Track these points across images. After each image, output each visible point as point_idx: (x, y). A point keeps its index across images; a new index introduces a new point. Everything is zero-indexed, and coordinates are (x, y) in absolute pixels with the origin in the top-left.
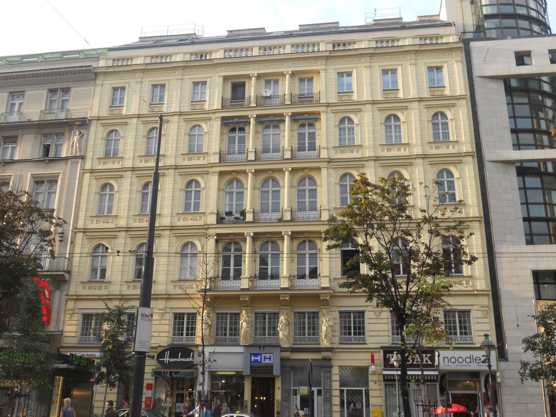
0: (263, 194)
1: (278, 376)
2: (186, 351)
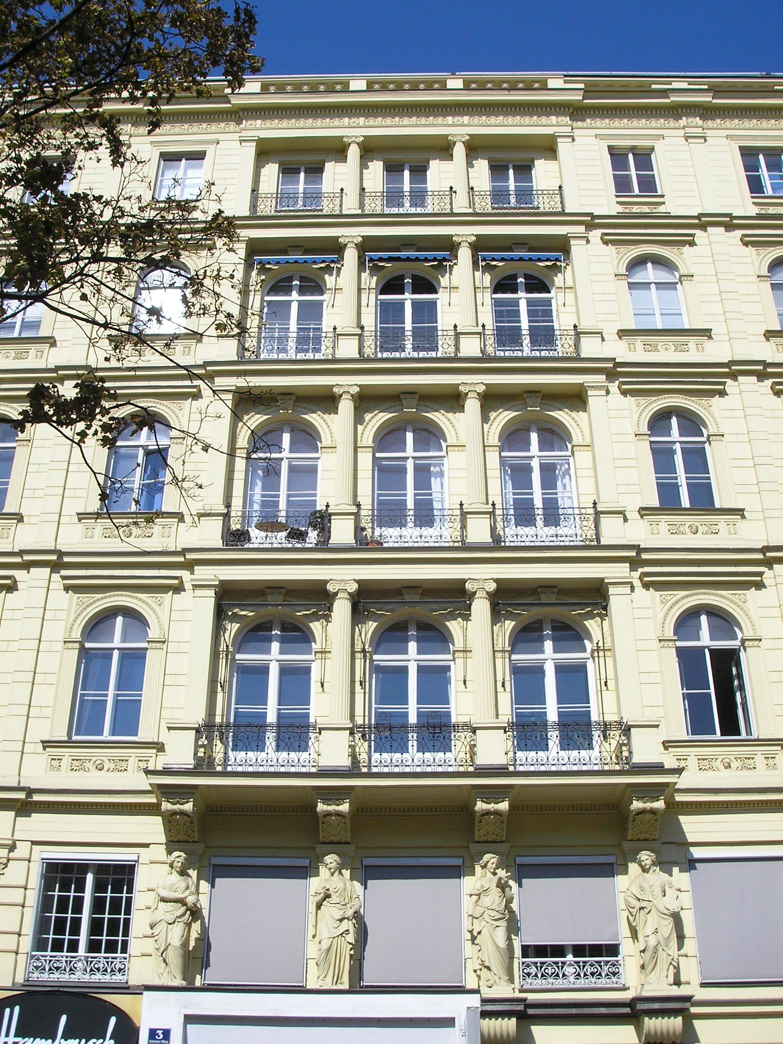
2: (499, 287)
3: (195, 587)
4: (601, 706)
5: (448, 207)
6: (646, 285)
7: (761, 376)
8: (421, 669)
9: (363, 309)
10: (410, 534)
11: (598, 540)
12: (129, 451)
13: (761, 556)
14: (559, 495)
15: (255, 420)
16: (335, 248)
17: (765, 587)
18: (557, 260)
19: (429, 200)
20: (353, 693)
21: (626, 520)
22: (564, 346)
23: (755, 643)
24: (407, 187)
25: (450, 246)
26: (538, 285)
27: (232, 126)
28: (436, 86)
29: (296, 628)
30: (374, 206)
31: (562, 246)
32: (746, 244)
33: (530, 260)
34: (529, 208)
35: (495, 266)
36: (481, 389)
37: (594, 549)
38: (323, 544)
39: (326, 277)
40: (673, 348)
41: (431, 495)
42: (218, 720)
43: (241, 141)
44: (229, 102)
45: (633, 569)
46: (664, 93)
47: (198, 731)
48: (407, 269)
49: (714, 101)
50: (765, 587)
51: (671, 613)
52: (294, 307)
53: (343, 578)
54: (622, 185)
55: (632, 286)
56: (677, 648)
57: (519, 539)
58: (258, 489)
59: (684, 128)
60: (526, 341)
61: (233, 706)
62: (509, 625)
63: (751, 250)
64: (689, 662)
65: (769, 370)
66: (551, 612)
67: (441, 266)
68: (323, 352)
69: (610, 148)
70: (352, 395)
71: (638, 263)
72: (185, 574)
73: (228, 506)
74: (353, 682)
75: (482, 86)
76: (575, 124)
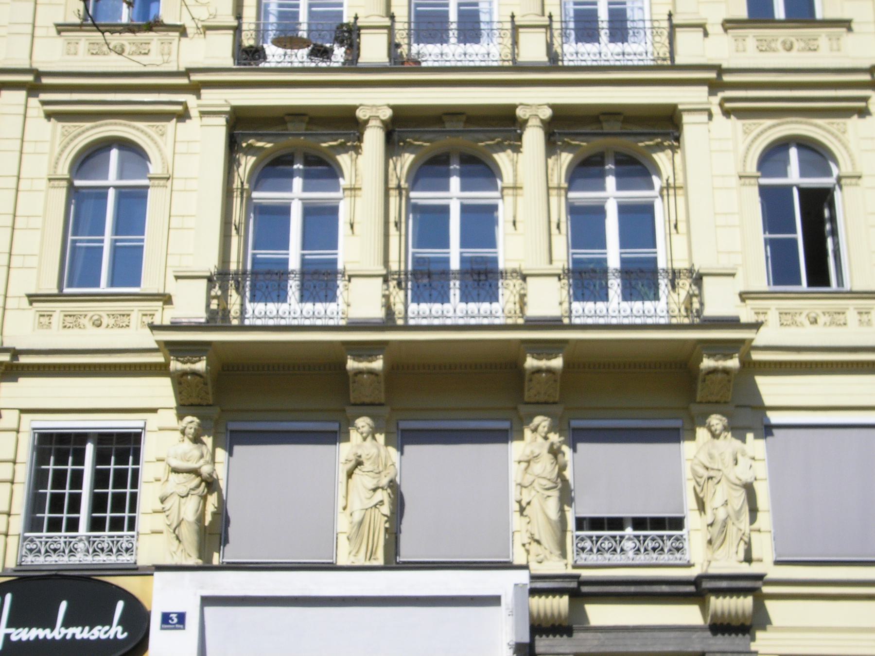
0: (209, 610)
1: (392, 189)
2: (91, 594)
3: (203, 114)
8: (466, 210)
10: (452, 52)
11: (672, 58)
23: (854, 181)
29: (320, 161)
37: (669, 71)
38: (352, 64)
42: (233, 267)
47: (210, 279)
53: (375, 103)
64: (774, 202)
72: (190, 99)
74: (549, 222)
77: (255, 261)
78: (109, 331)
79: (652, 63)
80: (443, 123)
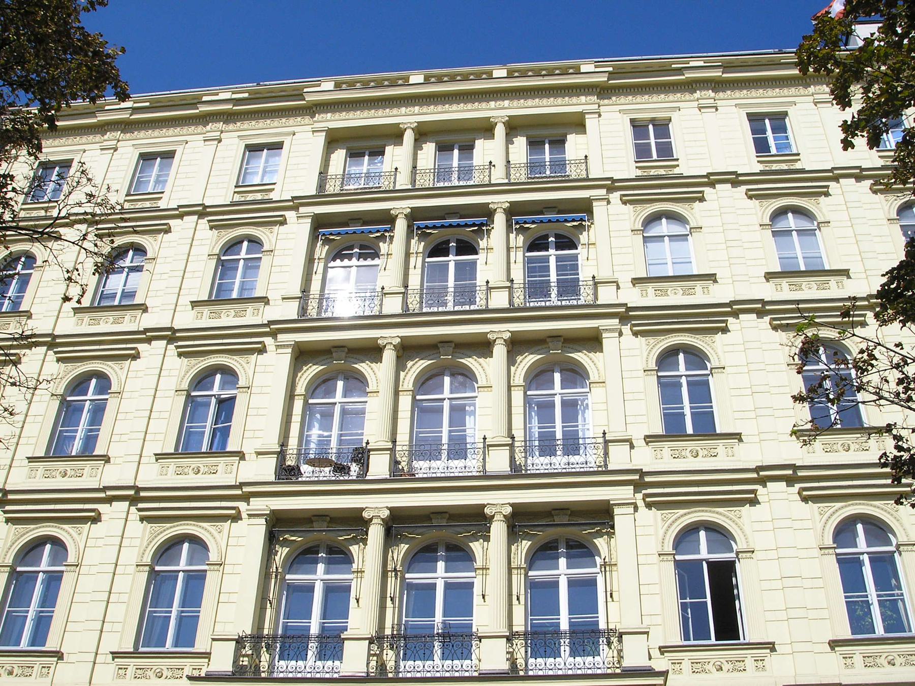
3: (250, 516)
4: (608, 616)
5: (584, 173)
6: (788, 233)
7: (760, 313)
8: (448, 586)
9: (512, 265)
10: (440, 466)
11: (606, 465)
12: (205, 399)
13: (755, 475)
14: (580, 427)
15: (311, 371)
16: (388, 219)
17: (759, 503)
18: (582, 220)
19: (476, 174)
20: (510, 605)
21: (632, 447)
22: (586, 296)
23: (748, 555)
24: (455, 163)
25: (487, 213)
26: (567, 242)
27: (307, 120)
28: (484, 76)
29: (341, 552)
30: (425, 181)
31: (585, 208)
32: (750, 197)
33: (558, 221)
34: (542, 178)
35: (528, 228)
36: (507, 335)
37: (604, 475)
38: (362, 478)
39: (381, 244)
40: (681, 292)
41: (465, 431)
42: (388, 632)
43: (313, 131)
44: (304, 100)
45: (636, 491)
46: (680, 71)
47: (371, 641)
48: (451, 233)
49: (724, 75)
50: (759, 503)
51: (669, 533)
52: (452, 266)
53: (376, 506)
54: (642, 152)
55: (775, 234)
56: (675, 561)
57: (535, 467)
58: (535, 420)
59: (698, 99)
60: (554, 293)
61: (281, 620)
62: (526, 544)
63: (755, 203)
64: (687, 574)
65: (767, 307)
66: (565, 532)
67: (483, 229)
68: (478, 303)
69: (749, 115)
70: (505, 340)
71: (654, 218)
72: (242, 506)
73: (394, 442)
74: (510, 595)
75: (523, 74)
76: (602, 102)
77: (286, 627)
78: (730, 675)
79: (478, 474)
80: (553, 516)
